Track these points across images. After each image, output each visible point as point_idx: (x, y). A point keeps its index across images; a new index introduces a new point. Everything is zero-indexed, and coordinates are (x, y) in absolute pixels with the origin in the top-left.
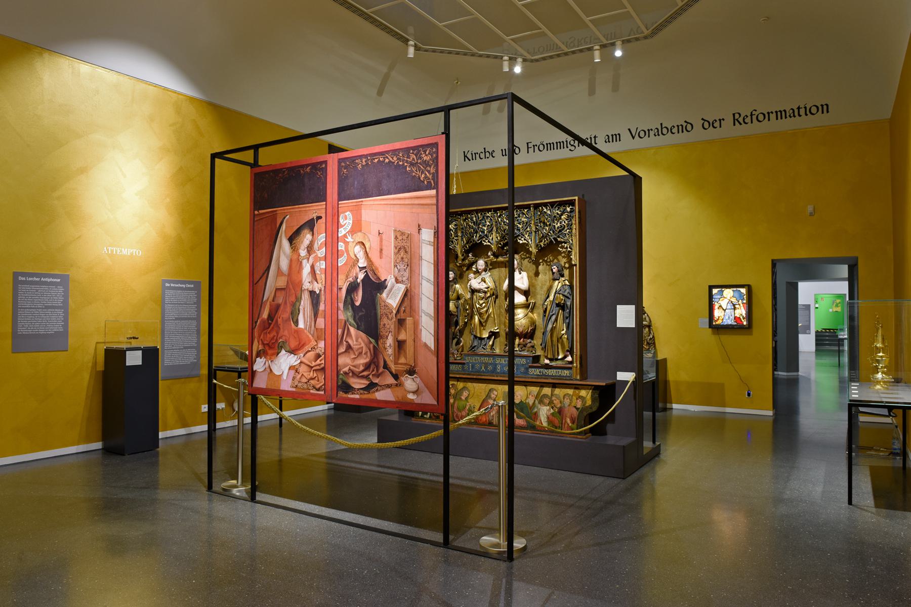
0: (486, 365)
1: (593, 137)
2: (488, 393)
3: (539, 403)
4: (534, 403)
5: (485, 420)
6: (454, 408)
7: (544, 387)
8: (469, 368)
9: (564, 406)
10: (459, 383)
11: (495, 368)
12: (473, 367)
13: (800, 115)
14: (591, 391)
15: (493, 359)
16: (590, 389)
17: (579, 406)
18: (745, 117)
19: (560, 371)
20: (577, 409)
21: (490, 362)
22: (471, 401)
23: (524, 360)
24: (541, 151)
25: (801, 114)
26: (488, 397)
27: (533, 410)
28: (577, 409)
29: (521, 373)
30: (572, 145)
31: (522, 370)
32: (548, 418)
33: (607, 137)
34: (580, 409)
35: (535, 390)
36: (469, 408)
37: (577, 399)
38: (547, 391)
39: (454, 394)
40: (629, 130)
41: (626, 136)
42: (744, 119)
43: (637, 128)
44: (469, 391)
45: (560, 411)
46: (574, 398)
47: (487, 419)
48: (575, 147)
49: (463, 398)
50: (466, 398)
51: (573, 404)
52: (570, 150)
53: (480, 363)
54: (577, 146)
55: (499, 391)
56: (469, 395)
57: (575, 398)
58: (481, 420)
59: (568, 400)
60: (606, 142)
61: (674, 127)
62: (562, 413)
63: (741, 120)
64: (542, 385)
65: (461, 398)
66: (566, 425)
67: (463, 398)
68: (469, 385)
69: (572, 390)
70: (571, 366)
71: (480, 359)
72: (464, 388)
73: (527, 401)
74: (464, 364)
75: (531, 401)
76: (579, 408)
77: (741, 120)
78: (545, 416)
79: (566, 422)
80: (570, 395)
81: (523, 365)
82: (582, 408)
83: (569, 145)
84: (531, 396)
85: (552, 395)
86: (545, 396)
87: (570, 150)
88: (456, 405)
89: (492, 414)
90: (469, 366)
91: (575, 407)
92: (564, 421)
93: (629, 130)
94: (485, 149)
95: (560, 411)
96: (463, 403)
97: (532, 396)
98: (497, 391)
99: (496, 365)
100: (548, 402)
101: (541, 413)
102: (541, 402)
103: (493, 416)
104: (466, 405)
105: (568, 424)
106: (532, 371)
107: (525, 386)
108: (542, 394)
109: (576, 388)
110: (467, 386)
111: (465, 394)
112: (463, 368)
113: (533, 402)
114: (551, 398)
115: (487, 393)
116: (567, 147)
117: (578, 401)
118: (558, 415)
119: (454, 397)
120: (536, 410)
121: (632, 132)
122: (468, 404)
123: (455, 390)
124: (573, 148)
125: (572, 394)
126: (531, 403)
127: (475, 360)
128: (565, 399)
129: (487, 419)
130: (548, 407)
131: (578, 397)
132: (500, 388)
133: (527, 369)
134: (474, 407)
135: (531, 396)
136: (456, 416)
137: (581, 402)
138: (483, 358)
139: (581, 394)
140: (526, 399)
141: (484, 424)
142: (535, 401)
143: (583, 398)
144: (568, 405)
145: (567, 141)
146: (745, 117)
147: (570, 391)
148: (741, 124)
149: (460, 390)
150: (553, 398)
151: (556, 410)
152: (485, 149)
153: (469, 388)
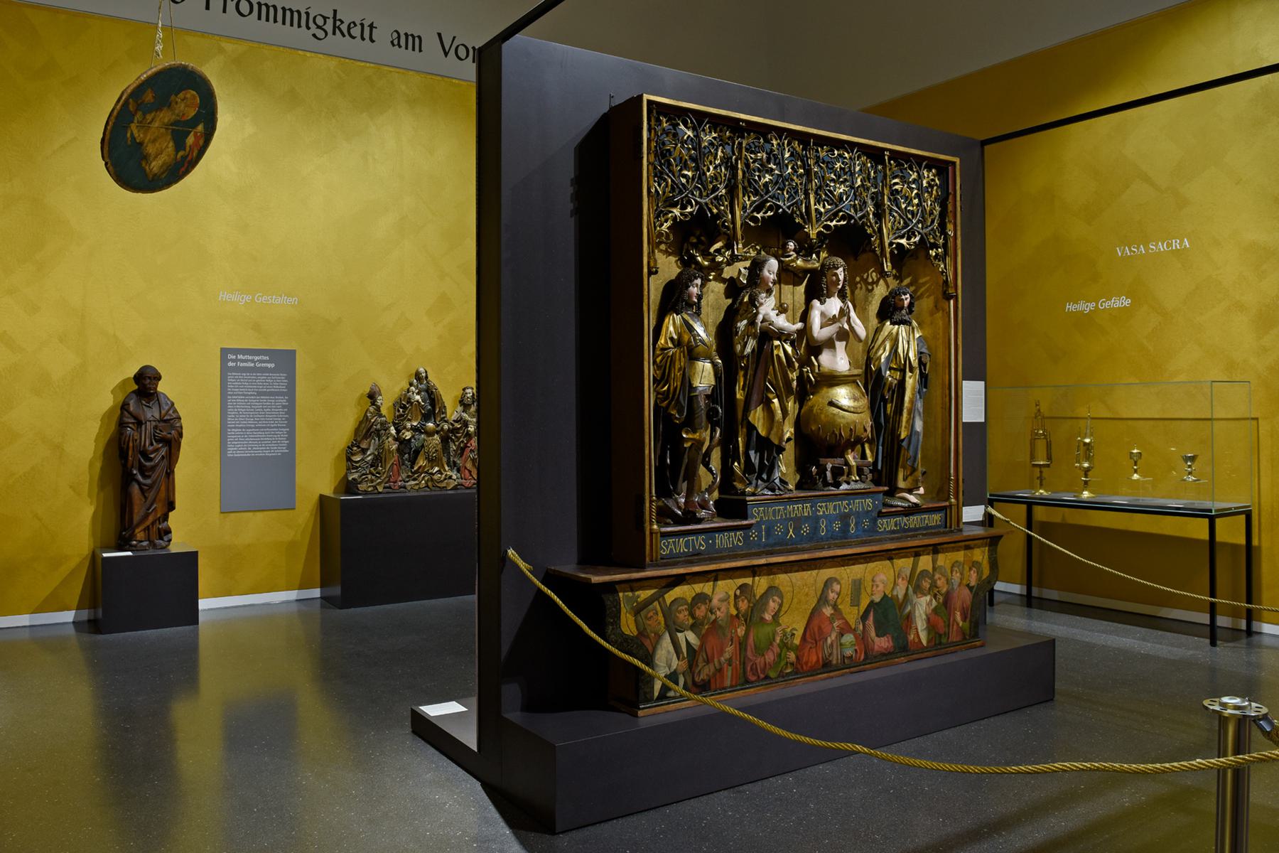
0: (798, 521)
1: (366, 23)
2: (823, 591)
3: (915, 592)
4: (906, 594)
5: (815, 659)
6: (746, 650)
7: (920, 555)
8: (760, 537)
9: (953, 588)
10: (757, 578)
11: (815, 529)
12: (769, 532)
13: (400, 47)
14: (987, 548)
15: (811, 507)
16: (986, 546)
17: (973, 583)
18: (352, 25)
19: (927, 516)
20: (971, 588)
21: (806, 514)
22: (784, 620)
23: (869, 501)
24: (242, 15)
25: (374, 38)
26: (821, 603)
27: (905, 608)
28: (971, 588)
29: (865, 531)
30: (319, 27)
31: (866, 523)
32: (928, 620)
33: (395, 35)
34: (975, 589)
35: (905, 564)
36: (781, 640)
37: (970, 569)
38: (925, 562)
39: (747, 611)
40: (439, 35)
41: (431, 44)
42: (349, 28)
43: (454, 37)
44: (781, 597)
45: (948, 598)
46: (967, 568)
47: (820, 656)
48: (326, 33)
49: (768, 617)
50: (776, 616)
51: (965, 582)
52: (314, 35)
53: (786, 519)
54: (330, 30)
55: (842, 582)
56: (781, 605)
57: (968, 569)
58: (806, 663)
59: (958, 574)
60: (393, 45)
61: (355, 25)
62: (948, 605)
63: (344, 28)
64: (916, 553)
65: (762, 619)
66: (955, 627)
67: (768, 617)
68: (782, 579)
69: (962, 553)
70: (947, 504)
71: (785, 509)
72: (772, 590)
73: (895, 593)
74: (749, 527)
75: (900, 592)
76: (973, 587)
77: (344, 28)
78: (924, 617)
79: (954, 620)
80: (960, 563)
81: (868, 511)
82: (978, 584)
83: (311, 24)
84: (900, 580)
85: (934, 569)
86: (924, 573)
87: (314, 35)
88: (751, 641)
89: (829, 641)
90: (760, 532)
91: (968, 585)
92: (951, 619)
93: (439, 35)
94: (335, 11)
95: (948, 598)
96: (768, 629)
97: (903, 579)
98: (839, 583)
99: (817, 519)
100: (928, 586)
101: (917, 612)
102: (918, 590)
103: (832, 645)
104: (774, 633)
105: (958, 624)
106: (886, 524)
107: (890, 559)
108: (918, 572)
109: (968, 548)
110: (777, 583)
111: (773, 605)
112: (746, 538)
113: (904, 592)
114: (933, 575)
115: (819, 593)
116: (308, 28)
117: (972, 572)
118: (943, 608)
119: (746, 621)
120: (909, 608)
121: (445, 44)
122: (779, 629)
123: (749, 602)
124: (320, 34)
125: (962, 559)
126: (901, 597)
127: (774, 516)
128: (954, 573)
129: (820, 656)
130: (928, 598)
131: (971, 565)
132: (845, 576)
133: (874, 521)
134: (793, 634)
135: (900, 580)
136: (751, 669)
137: (975, 575)
138: (790, 508)
139: (975, 558)
140: (893, 589)
141: (813, 672)
142: (907, 589)
143: (975, 565)
144: (957, 584)
145: (307, 14)
146: (352, 25)
147: (960, 556)
148: (344, 36)
149: (762, 597)
150: (937, 576)
151: (941, 601)
152: (335, 11)
153: (781, 588)
